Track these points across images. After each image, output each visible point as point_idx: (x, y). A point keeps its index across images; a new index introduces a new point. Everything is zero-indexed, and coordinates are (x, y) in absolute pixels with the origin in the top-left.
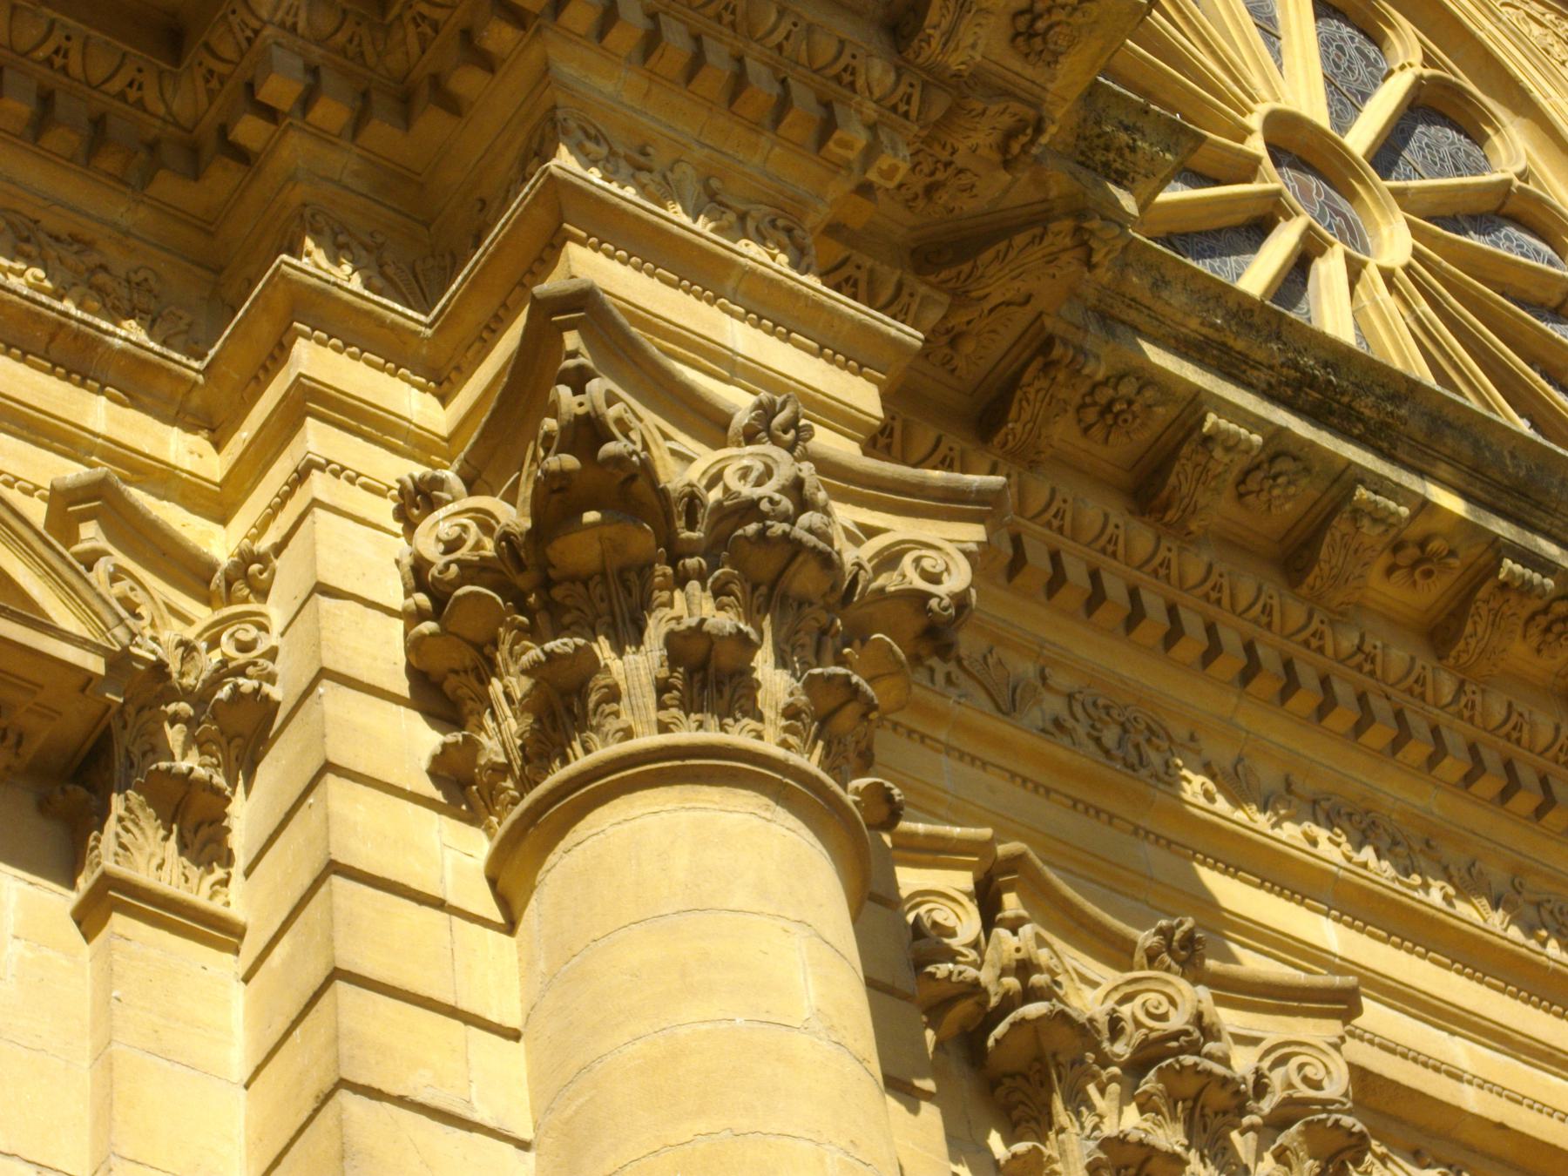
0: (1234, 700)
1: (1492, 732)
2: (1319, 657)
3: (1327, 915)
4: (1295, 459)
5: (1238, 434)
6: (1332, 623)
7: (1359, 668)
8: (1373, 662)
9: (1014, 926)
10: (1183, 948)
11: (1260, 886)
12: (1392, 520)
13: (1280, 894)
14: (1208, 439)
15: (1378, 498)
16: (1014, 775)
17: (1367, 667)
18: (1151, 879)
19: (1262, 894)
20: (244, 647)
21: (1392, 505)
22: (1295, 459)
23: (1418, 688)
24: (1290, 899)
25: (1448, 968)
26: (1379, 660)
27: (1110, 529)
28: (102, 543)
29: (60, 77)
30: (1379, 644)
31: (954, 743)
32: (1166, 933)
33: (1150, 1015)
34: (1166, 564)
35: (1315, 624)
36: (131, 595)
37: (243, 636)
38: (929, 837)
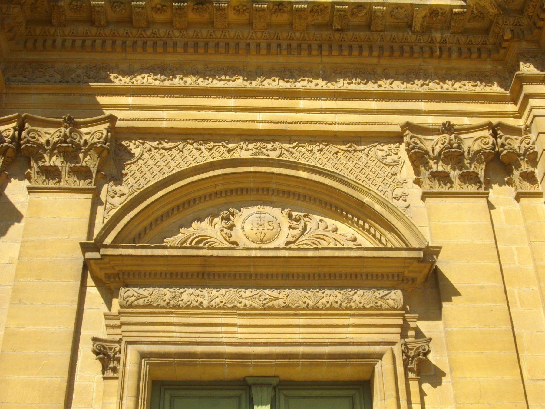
0: (124, 54)
1: (363, 41)
2: (143, 38)
3: (131, 96)
4: (117, 2)
5: (98, 4)
6: (422, 35)
7: (154, 37)
8: (156, 34)
9: (501, 137)
10: (69, 120)
11: (113, 96)
12: (142, 6)
13: (118, 96)
14: (375, 12)
15: (138, 3)
16: (50, 94)
17: (155, 36)
18: (82, 104)
19: (114, 97)
20: (528, 144)
21: (141, 3)
22: (117, 2)
23: (169, 36)
24: (104, 96)
25: (164, 97)
26: (157, 34)
27: (354, 36)
28: (502, 134)
29: (157, 38)
30: (157, 30)
31: (36, 92)
32: (65, 118)
33: (485, 145)
34: (100, 33)
35: (418, 38)
36: (415, 141)
37: (527, 142)
38: (8, 118)
